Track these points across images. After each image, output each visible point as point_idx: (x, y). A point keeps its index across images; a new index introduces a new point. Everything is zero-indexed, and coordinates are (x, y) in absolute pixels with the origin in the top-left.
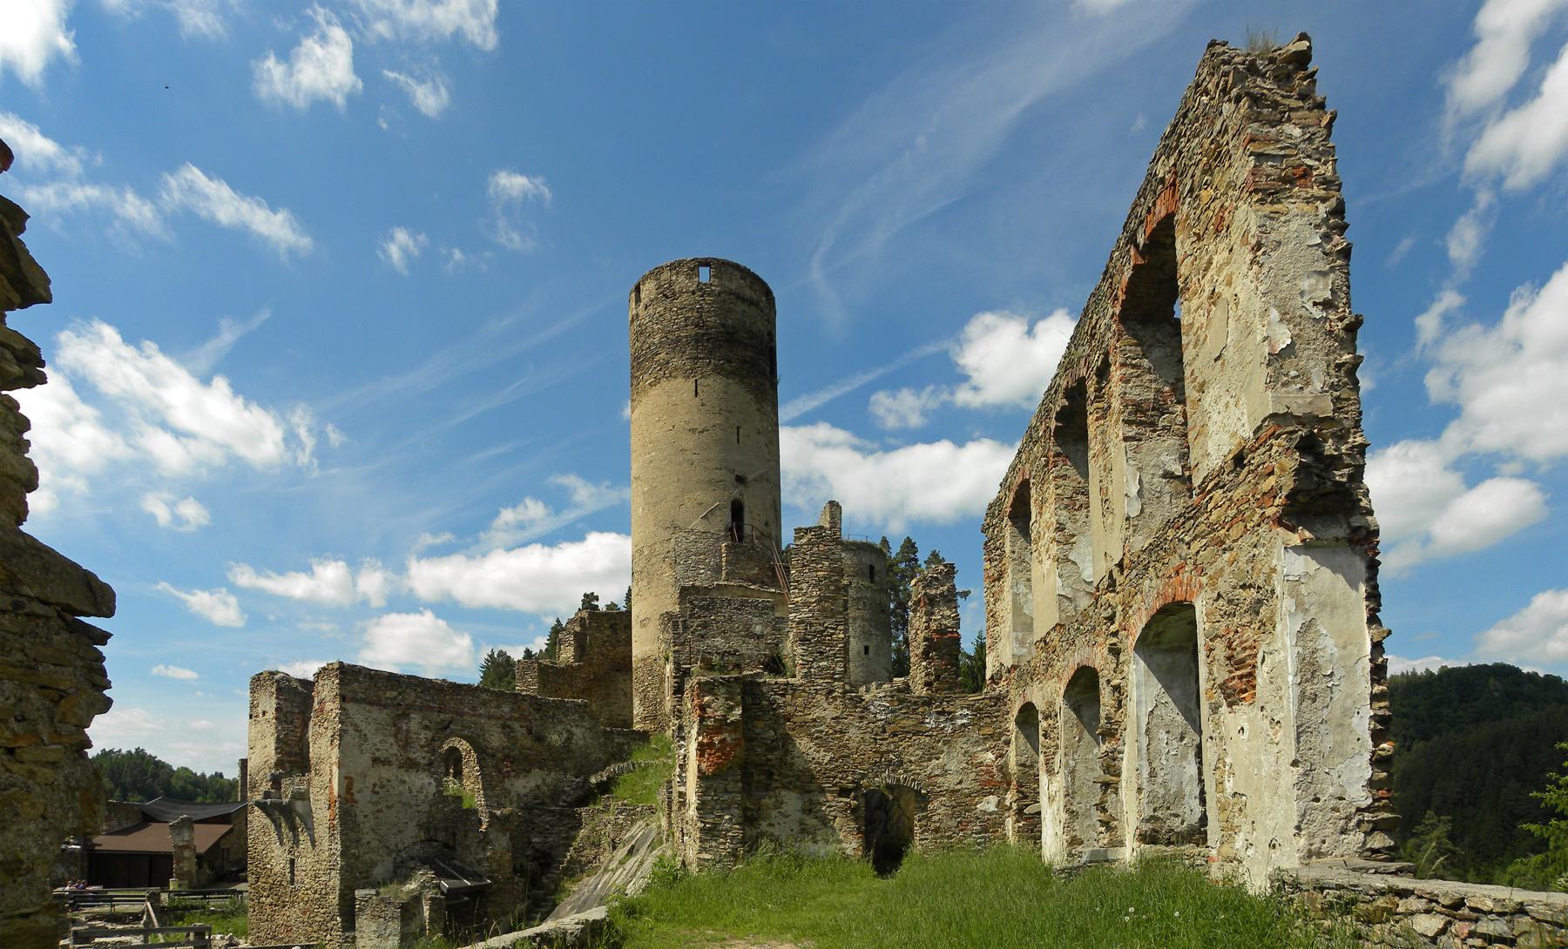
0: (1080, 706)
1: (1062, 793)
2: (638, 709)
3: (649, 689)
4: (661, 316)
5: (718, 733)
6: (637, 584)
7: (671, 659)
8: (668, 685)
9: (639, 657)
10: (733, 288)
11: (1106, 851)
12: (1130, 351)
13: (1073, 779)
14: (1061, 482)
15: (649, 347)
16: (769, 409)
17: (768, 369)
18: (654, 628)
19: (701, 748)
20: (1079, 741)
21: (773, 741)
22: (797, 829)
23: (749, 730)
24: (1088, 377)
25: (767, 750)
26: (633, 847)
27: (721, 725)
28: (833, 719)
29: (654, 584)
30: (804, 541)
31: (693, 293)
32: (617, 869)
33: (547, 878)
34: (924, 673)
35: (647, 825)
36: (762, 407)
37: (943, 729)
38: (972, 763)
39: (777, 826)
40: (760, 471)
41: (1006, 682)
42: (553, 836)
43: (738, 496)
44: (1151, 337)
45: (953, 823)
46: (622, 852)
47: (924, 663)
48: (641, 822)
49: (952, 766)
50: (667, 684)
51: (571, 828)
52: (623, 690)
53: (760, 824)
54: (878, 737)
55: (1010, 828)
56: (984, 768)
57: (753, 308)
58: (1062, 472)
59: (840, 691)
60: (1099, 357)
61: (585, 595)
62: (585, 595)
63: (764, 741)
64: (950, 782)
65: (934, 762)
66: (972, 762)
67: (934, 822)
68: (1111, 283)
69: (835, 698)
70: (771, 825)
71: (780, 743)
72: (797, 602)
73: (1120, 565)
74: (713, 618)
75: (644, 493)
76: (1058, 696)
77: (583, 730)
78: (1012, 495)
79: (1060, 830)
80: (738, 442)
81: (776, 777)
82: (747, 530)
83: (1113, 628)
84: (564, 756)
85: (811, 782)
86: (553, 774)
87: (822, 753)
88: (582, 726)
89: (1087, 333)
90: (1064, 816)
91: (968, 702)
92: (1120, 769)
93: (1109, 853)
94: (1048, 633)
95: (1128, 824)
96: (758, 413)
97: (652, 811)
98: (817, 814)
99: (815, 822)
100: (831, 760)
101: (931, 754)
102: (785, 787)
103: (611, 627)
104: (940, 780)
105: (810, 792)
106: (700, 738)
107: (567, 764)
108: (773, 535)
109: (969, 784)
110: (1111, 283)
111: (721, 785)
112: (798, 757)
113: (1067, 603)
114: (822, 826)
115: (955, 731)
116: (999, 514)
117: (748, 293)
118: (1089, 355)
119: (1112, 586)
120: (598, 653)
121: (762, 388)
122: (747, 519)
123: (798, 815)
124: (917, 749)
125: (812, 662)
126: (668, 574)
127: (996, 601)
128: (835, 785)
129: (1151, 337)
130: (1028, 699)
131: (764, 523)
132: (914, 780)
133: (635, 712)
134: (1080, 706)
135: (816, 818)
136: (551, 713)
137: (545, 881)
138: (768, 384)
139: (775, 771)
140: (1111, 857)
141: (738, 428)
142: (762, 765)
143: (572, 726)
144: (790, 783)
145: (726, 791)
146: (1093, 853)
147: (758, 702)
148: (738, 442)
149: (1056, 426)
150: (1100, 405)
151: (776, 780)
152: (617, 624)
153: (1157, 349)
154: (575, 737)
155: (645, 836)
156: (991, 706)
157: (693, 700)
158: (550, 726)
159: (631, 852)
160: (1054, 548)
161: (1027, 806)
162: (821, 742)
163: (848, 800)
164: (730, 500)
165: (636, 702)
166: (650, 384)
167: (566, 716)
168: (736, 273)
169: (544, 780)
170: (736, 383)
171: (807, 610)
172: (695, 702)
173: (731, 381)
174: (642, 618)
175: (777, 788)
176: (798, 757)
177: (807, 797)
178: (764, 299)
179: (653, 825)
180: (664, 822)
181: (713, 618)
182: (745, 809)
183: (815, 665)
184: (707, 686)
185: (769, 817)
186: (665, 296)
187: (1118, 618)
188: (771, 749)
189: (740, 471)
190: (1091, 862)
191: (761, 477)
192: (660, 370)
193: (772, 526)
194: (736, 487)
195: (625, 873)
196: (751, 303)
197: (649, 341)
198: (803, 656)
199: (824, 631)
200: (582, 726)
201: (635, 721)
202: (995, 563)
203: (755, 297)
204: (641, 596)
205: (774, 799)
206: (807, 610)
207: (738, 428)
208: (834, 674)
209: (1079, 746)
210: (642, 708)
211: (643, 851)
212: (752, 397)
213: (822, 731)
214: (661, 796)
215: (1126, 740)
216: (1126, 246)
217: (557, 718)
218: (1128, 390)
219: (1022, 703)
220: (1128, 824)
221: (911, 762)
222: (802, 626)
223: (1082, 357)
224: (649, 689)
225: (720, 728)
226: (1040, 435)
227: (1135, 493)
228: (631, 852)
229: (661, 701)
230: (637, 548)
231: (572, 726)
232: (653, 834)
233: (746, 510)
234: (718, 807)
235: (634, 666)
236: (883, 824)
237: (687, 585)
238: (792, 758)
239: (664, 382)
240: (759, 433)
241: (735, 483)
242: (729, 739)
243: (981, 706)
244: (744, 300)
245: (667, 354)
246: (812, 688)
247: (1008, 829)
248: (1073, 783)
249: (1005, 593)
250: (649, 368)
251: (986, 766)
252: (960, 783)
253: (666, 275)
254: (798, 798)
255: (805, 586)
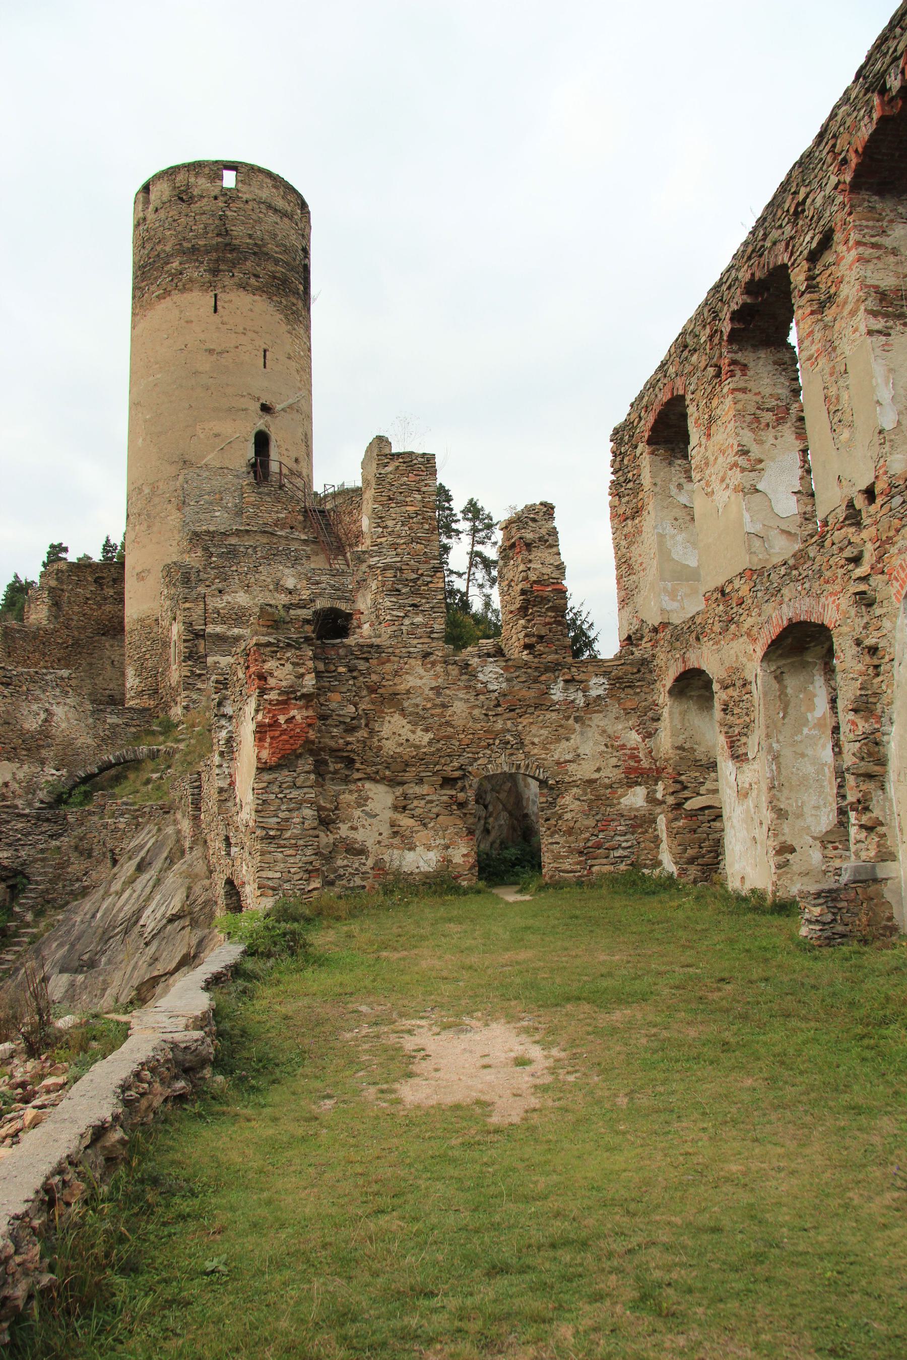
0: (782, 673)
1: (764, 787)
2: (132, 681)
3: (148, 656)
4: (174, 221)
5: (284, 711)
6: (134, 529)
7: (180, 618)
8: (176, 650)
9: (135, 617)
10: (264, 196)
11: (873, 868)
12: (867, 227)
13: (778, 768)
14: (740, 395)
15: (158, 255)
16: (302, 332)
17: (301, 287)
18: (155, 580)
19: (261, 732)
20: (784, 718)
21: (353, 719)
22: (386, 831)
23: (322, 705)
24: (793, 264)
25: (346, 731)
26: (143, 859)
27: (290, 696)
28: (432, 689)
29: (155, 529)
30: (389, 469)
31: (216, 198)
32: (123, 891)
33: (21, 905)
34: (523, 634)
35: (159, 830)
36: (294, 329)
37: (573, 701)
38: (612, 746)
39: (361, 830)
40: (291, 401)
41: (649, 644)
42: (27, 848)
43: (263, 428)
44: (891, 211)
45: (591, 822)
46: (129, 867)
47: (522, 622)
48: (150, 827)
49: (587, 749)
50: (172, 649)
51: (51, 836)
52: (110, 658)
53: (339, 828)
54: (490, 713)
55: (664, 828)
56: (628, 752)
57: (286, 220)
58: (742, 385)
59: (440, 654)
60: (812, 238)
61: (52, 547)
62: (52, 547)
63: (341, 719)
64: (584, 771)
65: (564, 744)
66: (613, 744)
67: (567, 820)
68: (834, 146)
69: (433, 664)
70: (353, 828)
71: (363, 722)
72: (381, 544)
73: (870, 494)
74: (234, 568)
75: (146, 421)
76: (750, 659)
77: (67, 708)
78: (651, 418)
79: (761, 833)
80: (265, 367)
81: (358, 765)
82: (274, 467)
83: (860, 571)
84: (41, 743)
85: (405, 771)
86: (26, 767)
87: (419, 733)
88: (65, 704)
89: (788, 211)
90: (768, 816)
91: (604, 669)
92: (885, 756)
93: (878, 870)
94: (730, 581)
95: (901, 830)
96: (289, 335)
97: (166, 810)
98: (413, 812)
99: (411, 822)
100: (430, 743)
101: (560, 734)
102: (369, 778)
103: (95, 581)
104: (571, 767)
105: (402, 783)
106: (260, 717)
107: (44, 753)
108: (304, 474)
109: (610, 774)
110: (834, 146)
111: (288, 779)
112: (387, 739)
113: (757, 543)
114: (421, 828)
115: (588, 705)
116: (629, 441)
117: (280, 203)
118: (792, 238)
119: (853, 517)
120: (79, 613)
121: (294, 308)
122: (274, 454)
123: (388, 814)
124: (542, 728)
125: (403, 617)
126: (174, 518)
127: (631, 543)
128: (435, 773)
129: (891, 211)
130: (693, 663)
131: (294, 459)
132: (538, 767)
133: (128, 685)
134: (782, 673)
135: (413, 817)
136: (25, 688)
137: (17, 909)
138: (300, 304)
139: (356, 758)
140: (880, 875)
141: (265, 351)
142: (339, 750)
143: (52, 704)
144: (377, 773)
145: (294, 786)
146: (857, 870)
147: (334, 668)
148: (265, 367)
149: (732, 329)
150: (815, 296)
151: (358, 770)
152: (103, 578)
153: (901, 226)
154: (55, 718)
155: (158, 846)
156: (632, 674)
157: (248, 668)
158: (24, 704)
159: (141, 868)
160: (736, 477)
161: (687, 799)
162: (417, 719)
163: (453, 792)
164: (254, 433)
165: (130, 672)
166: (157, 297)
167: (44, 691)
168: (268, 181)
169: (14, 774)
170: (263, 300)
171: (394, 553)
172: (252, 670)
173: (257, 298)
174: (139, 569)
175: (360, 779)
176: (387, 739)
177: (399, 791)
178: (299, 211)
179: (170, 830)
180: (186, 825)
181: (234, 568)
182: (320, 809)
183: (407, 622)
184: (268, 649)
185: (350, 818)
186: (181, 199)
187: (869, 558)
188: (351, 730)
189: (266, 399)
190: (855, 882)
191: (290, 407)
192: (172, 280)
193: (303, 464)
194: (261, 417)
195: (135, 895)
196: (284, 214)
197: (159, 248)
198: (392, 609)
199: (418, 579)
200: (65, 704)
201: (128, 696)
202: (626, 498)
203: (289, 209)
204: (138, 543)
205: (356, 795)
206: (394, 553)
207: (265, 351)
208: (432, 632)
209: (783, 724)
210: (138, 680)
211: (158, 864)
212: (282, 316)
213: (417, 705)
214: (185, 788)
215: (894, 717)
216: (865, 95)
217: (33, 695)
218: (869, 274)
219: (681, 670)
220: (901, 830)
221: (533, 744)
222: (390, 573)
223: (780, 241)
224: (148, 656)
225: (286, 704)
226: (702, 341)
227: (889, 401)
228: (141, 868)
229: (165, 670)
230: (136, 485)
231: (52, 704)
232: (170, 843)
233: (273, 445)
234: (284, 807)
235: (127, 628)
236: (482, 822)
237: (198, 529)
238: (379, 741)
239: (176, 297)
240: (289, 358)
241: (260, 413)
242: (298, 717)
243: (621, 674)
244: (276, 211)
245: (181, 264)
246: (404, 650)
247: (662, 830)
248: (779, 772)
249: (644, 534)
250: (156, 279)
251: (631, 749)
252: (598, 770)
253: (180, 178)
254: (388, 792)
255: (390, 523)
